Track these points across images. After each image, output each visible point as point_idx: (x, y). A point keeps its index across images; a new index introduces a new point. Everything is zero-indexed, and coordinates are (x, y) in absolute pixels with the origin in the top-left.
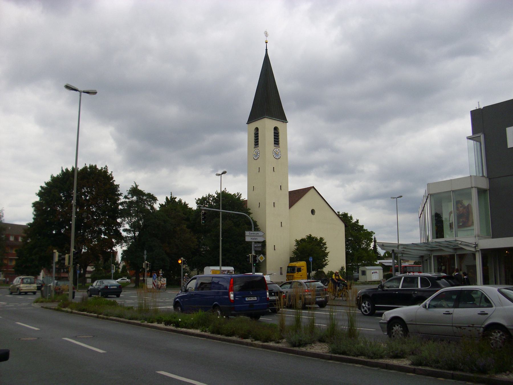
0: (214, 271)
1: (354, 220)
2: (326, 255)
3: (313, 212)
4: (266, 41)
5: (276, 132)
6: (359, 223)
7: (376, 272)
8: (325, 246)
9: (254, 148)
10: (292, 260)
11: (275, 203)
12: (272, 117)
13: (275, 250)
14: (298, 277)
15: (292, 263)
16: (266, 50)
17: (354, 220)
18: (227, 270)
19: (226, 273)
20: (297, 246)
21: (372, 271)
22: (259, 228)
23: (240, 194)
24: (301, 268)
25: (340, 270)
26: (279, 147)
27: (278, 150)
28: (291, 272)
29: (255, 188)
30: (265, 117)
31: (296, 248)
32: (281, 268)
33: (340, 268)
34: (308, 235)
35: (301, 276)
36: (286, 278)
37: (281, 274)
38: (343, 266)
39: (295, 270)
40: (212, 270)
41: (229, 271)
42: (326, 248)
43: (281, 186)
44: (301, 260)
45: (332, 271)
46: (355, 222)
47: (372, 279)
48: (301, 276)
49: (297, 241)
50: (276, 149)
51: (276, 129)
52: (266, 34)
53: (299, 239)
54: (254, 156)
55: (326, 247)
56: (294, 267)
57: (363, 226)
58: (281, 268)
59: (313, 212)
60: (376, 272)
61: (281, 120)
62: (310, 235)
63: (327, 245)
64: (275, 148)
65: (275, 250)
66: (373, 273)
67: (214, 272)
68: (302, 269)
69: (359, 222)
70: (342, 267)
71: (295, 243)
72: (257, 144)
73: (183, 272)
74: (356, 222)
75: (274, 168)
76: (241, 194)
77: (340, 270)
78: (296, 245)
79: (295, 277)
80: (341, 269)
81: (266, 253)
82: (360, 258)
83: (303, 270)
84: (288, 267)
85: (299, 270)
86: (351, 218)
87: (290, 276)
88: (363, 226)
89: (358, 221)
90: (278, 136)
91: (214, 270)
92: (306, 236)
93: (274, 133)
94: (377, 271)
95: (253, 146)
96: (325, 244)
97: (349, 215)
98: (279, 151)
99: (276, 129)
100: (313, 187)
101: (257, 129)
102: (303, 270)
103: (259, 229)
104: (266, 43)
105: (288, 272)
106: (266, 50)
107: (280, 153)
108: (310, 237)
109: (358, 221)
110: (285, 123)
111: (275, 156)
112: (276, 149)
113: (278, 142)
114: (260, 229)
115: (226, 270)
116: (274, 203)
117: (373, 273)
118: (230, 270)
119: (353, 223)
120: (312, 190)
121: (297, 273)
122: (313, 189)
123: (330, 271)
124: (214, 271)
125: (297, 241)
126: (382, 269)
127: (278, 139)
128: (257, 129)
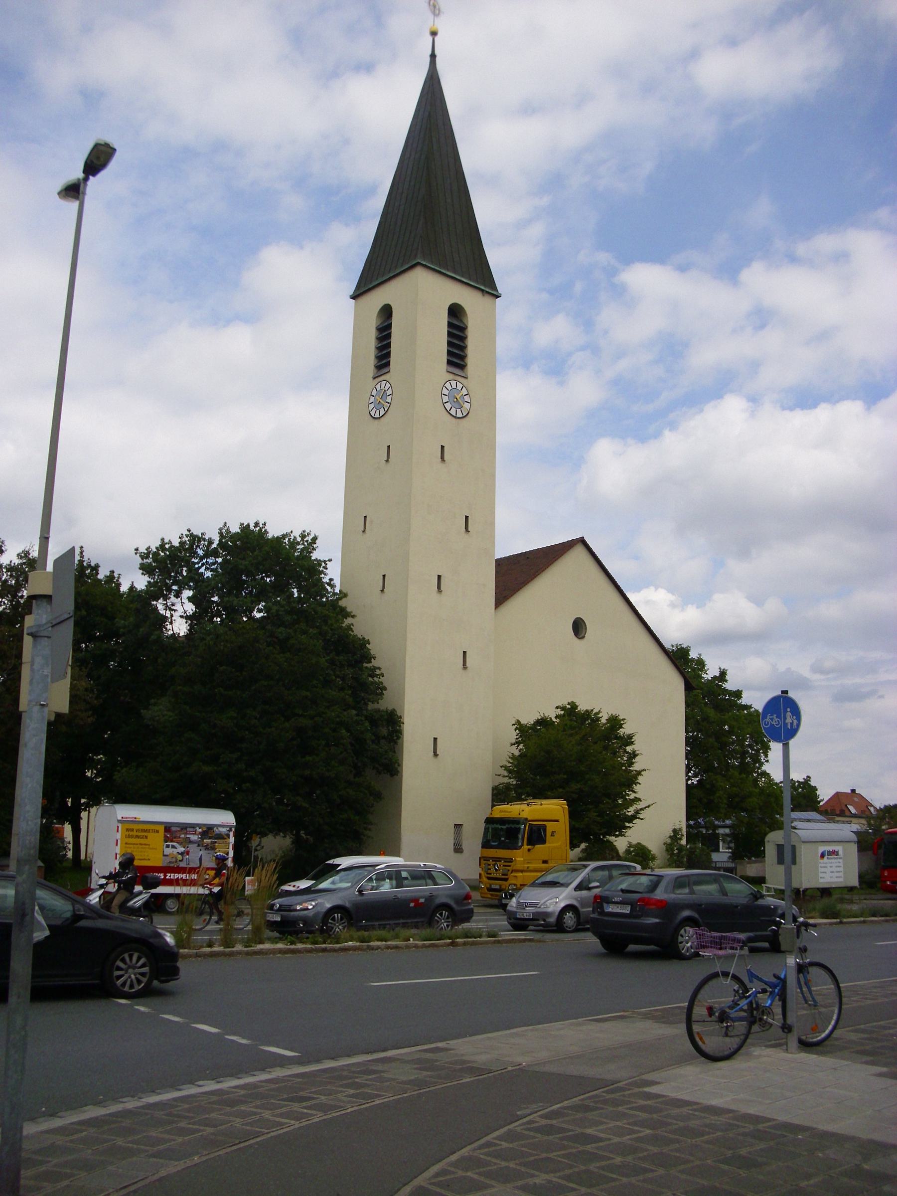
0: (135, 827)
1: (711, 672)
2: (631, 780)
3: (579, 627)
4: (434, 29)
5: (456, 322)
6: (726, 681)
7: (835, 853)
8: (629, 749)
9: (374, 378)
10: (500, 795)
11: (442, 578)
12: (444, 268)
13: (436, 754)
14: (532, 866)
15: (508, 806)
16: (433, 56)
17: (711, 672)
18: (200, 826)
19: (194, 838)
20: (521, 746)
21: (822, 849)
22: (379, 669)
23: (309, 538)
24: (544, 827)
25: (669, 841)
26: (466, 378)
27: (460, 386)
28: (502, 846)
29: (371, 522)
30: (418, 264)
31: (517, 753)
32: (458, 827)
33: (668, 836)
34: (564, 702)
35: (545, 862)
36: (480, 870)
37: (458, 849)
38: (677, 827)
39: (520, 836)
40: (122, 821)
41: (208, 831)
42: (634, 755)
43: (467, 517)
44: (540, 793)
45: (644, 843)
46: (715, 678)
47: (821, 880)
48: (545, 862)
49: (521, 728)
50: (453, 383)
51: (455, 312)
52: (435, 6)
53: (529, 719)
54: (372, 406)
55: (634, 752)
56: (516, 821)
57: (738, 694)
58: (458, 827)
59: (579, 627)
60: (835, 853)
61: (477, 282)
62: (574, 706)
63: (638, 746)
64: (451, 376)
65: (436, 754)
66: (822, 856)
67: (135, 833)
68: (549, 833)
69: (727, 678)
70: (675, 831)
71: (512, 735)
72: (384, 362)
73: (618, 860)
74: (715, 677)
75: (442, 447)
76: (315, 539)
77: (669, 841)
78: (517, 743)
79: (519, 866)
80: (670, 837)
81: (400, 765)
82: (737, 799)
83: (552, 835)
84: (489, 821)
85: (537, 835)
86: (701, 663)
87: (498, 859)
88: (738, 694)
89: (723, 675)
90: (463, 339)
91: (135, 821)
92: (557, 708)
93: (450, 325)
94: (838, 848)
95: (371, 370)
96: (628, 740)
97: (693, 655)
98: (464, 392)
99: (455, 312)
100: (582, 541)
101: (387, 312)
102: (552, 835)
103: (378, 672)
104: (434, 34)
105: (486, 845)
106: (433, 56)
107: (467, 398)
108: (570, 712)
109: (723, 675)
110: (488, 299)
111: (448, 406)
112: (453, 383)
113: (463, 358)
114: (382, 671)
115: (193, 826)
116: (439, 577)
117: (822, 856)
118: (218, 826)
119: (708, 680)
120: (579, 552)
121: (526, 847)
122: (579, 550)
123: (634, 842)
124: (135, 827)
125: (521, 728)
126: (856, 839)
127: (463, 348)
128: (387, 312)
